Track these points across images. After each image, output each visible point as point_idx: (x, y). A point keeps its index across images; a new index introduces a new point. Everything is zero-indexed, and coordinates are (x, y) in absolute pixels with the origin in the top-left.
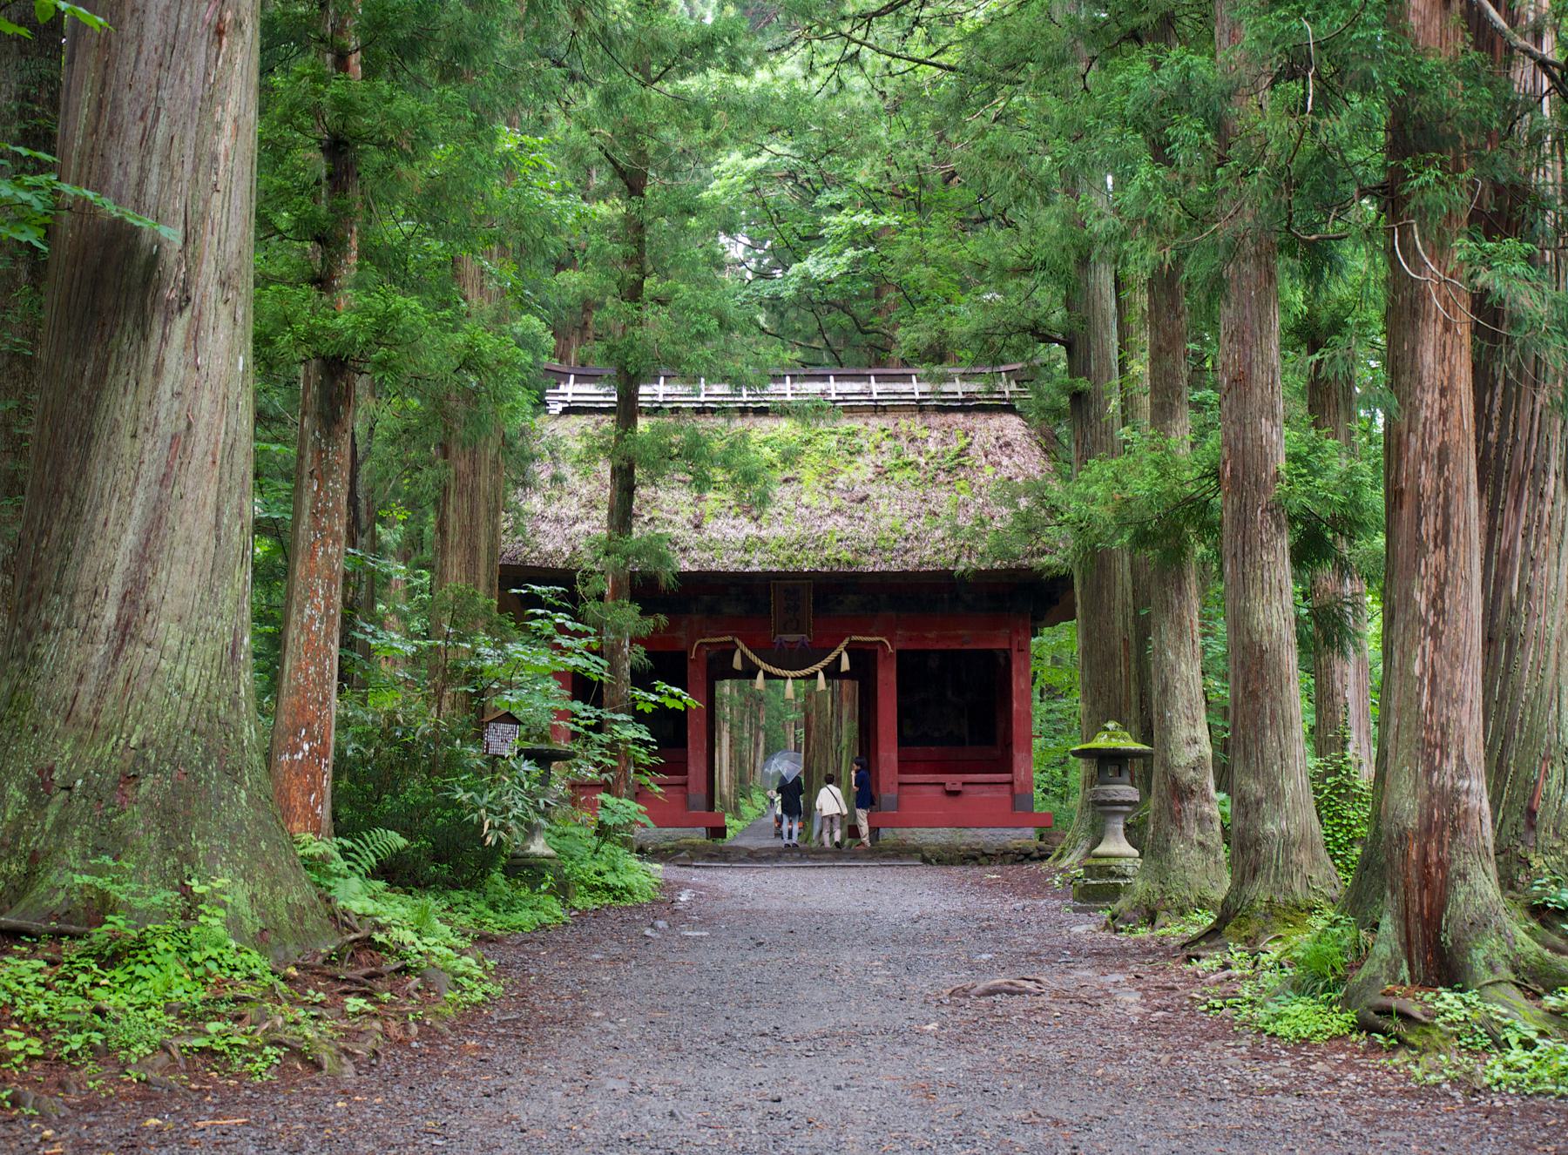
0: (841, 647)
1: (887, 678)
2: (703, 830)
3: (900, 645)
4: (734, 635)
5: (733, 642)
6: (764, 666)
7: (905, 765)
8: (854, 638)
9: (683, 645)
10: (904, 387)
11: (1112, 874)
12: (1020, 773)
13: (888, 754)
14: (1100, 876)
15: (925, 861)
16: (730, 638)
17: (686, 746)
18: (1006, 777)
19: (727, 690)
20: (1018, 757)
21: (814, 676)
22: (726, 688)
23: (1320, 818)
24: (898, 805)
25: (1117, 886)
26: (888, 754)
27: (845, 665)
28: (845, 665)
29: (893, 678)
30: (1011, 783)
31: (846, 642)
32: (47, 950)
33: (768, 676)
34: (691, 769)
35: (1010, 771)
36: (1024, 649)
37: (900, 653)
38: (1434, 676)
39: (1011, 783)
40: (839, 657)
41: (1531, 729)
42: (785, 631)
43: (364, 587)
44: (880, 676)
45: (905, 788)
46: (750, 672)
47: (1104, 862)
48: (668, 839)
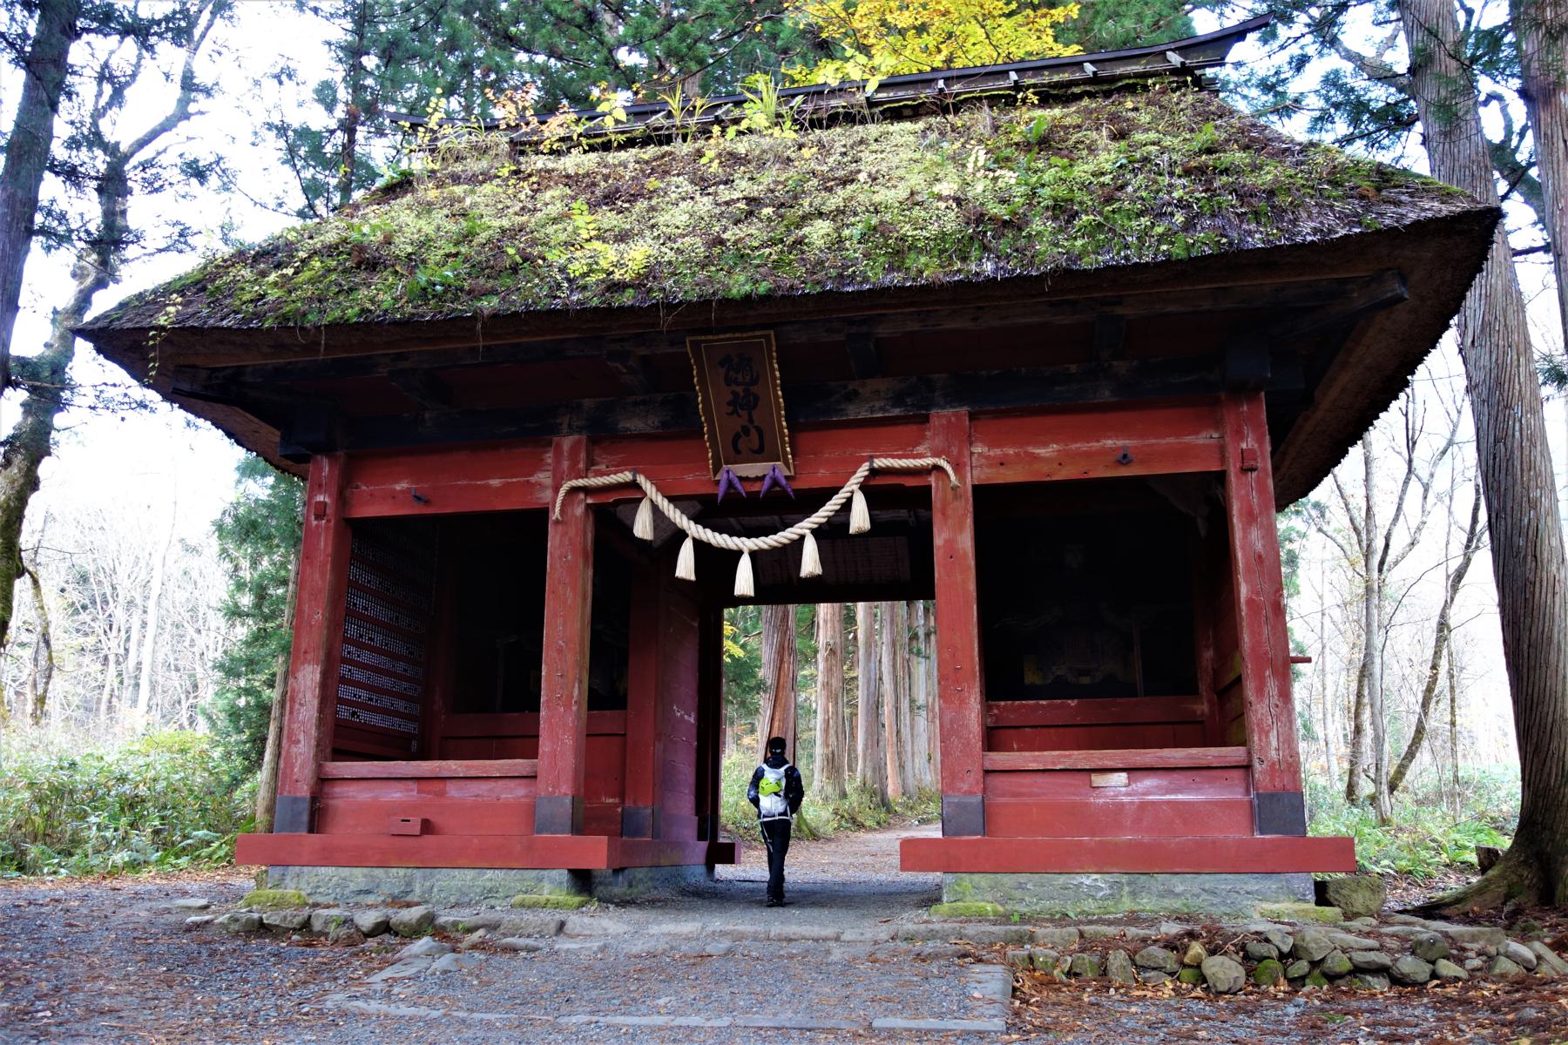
0: (853, 484)
2: (562, 875)
4: (635, 472)
5: (634, 485)
8: (880, 463)
9: (547, 495)
12: (1269, 746)
16: (627, 476)
17: (539, 711)
18: (1234, 754)
20: (1260, 710)
29: (966, 541)
31: (863, 472)
32: (271, 944)
34: (545, 746)
38: (1367, 557)
39: (1247, 768)
40: (847, 506)
41: (1508, 897)
42: (738, 456)
45: (997, 781)
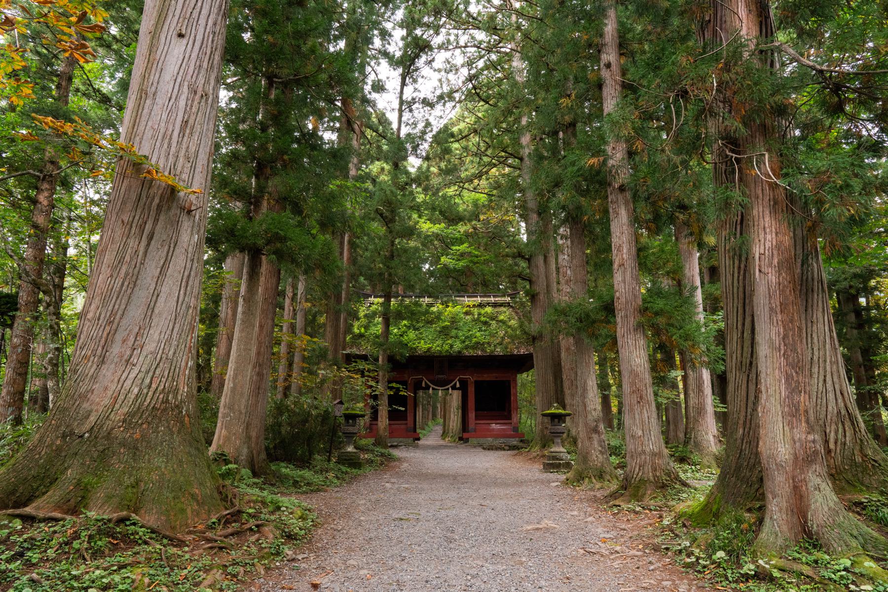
1: (471, 390)
3: (475, 379)
6: (432, 386)
7: (477, 418)
10: (489, 299)
11: (557, 459)
13: (472, 415)
14: (553, 460)
15: (484, 449)
19: (421, 394)
21: (448, 389)
22: (421, 393)
23: (44, 494)
24: (475, 431)
25: (560, 463)
26: (472, 415)
27: (458, 385)
28: (458, 385)
29: (473, 389)
30: (406, 424)
33: (433, 389)
34: (408, 419)
35: (511, 419)
36: (515, 380)
37: (476, 382)
40: (456, 383)
43: (103, 339)
44: (469, 389)
46: (428, 388)
47: (554, 454)
48: (850, 428)
